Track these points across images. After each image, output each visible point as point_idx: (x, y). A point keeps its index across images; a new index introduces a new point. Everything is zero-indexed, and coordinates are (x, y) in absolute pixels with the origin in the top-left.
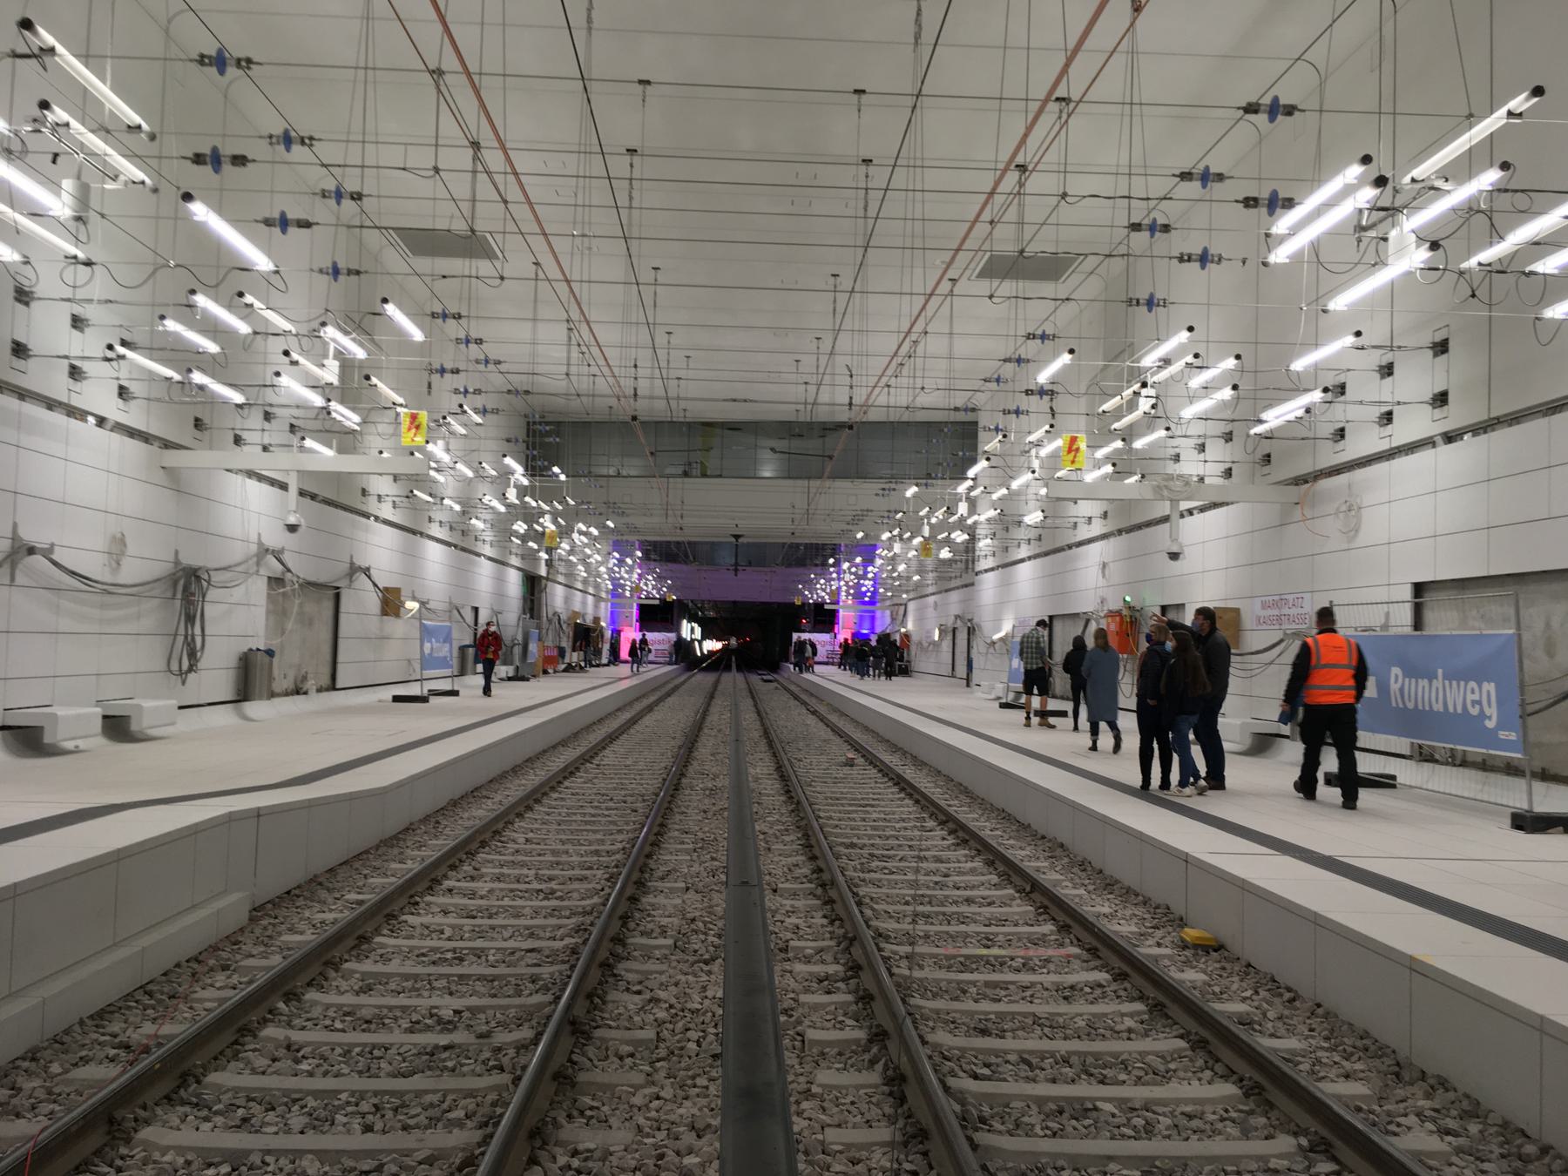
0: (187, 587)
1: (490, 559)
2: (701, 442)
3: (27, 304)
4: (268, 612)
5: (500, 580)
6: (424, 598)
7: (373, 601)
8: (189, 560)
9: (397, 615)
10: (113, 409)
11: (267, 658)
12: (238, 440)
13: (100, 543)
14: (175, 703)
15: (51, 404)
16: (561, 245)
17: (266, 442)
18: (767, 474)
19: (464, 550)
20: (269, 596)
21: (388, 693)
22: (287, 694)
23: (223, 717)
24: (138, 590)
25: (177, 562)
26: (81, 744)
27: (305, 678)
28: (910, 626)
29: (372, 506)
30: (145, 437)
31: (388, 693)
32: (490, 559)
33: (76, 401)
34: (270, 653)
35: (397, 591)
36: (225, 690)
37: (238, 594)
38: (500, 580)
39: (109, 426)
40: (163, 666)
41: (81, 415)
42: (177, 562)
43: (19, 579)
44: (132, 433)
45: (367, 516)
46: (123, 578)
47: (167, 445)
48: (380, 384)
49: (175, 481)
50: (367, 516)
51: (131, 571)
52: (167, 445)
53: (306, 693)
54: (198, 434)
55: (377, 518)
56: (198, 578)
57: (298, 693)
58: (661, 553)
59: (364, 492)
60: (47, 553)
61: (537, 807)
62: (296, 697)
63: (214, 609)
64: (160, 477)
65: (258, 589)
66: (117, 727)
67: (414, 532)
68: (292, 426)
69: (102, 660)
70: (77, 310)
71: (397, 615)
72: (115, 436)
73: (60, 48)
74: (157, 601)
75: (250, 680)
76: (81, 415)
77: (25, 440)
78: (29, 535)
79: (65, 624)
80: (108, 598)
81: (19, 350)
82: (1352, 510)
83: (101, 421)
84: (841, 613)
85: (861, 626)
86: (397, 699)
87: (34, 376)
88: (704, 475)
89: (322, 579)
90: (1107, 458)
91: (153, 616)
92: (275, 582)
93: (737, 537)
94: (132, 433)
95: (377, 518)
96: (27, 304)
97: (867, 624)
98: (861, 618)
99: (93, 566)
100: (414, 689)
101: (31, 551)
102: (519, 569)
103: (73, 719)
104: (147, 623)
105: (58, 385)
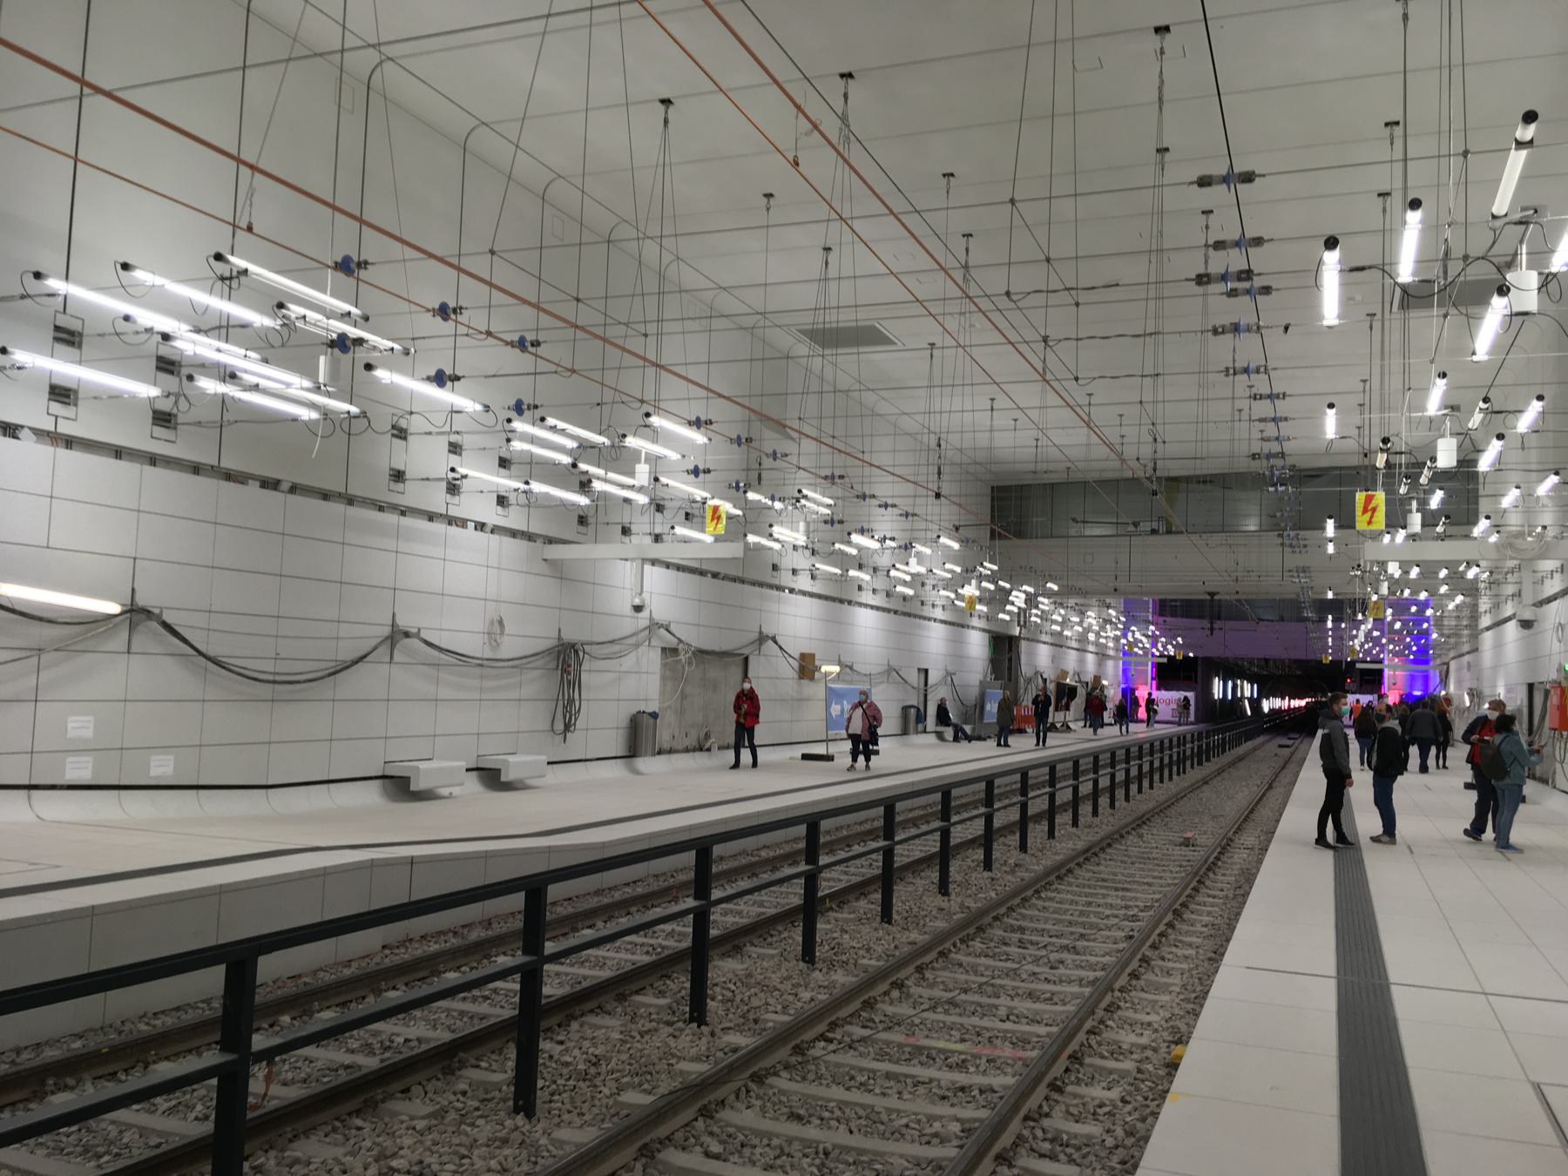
0: (566, 659)
1: (942, 622)
2: (1169, 497)
3: (405, 439)
4: (663, 678)
5: (957, 644)
6: (846, 659)
7: (788, 670)
8: (569, 636)
9: (812, 678)
10: (493, 515)
11: (651, 721)
12: (626, 531)
13: (480, 625)
14: (544, 758)
15: (431, 517)
16: (951, 323)
17: (657, 531)
18: (1252, 528)
19: (905, 614)
20: (664, 665)
21: (799, 751)
22: (687, 750)
23: (615, 770)
24: (520, 663)
25: (559, 638)
26: (456, 791)
27: (707, 736)
28: (1452, 688)
29: (786, 579)
30: (529, 537)
31: (799, 751)
32: (942, 622)
33: (453, 512)
34: (654, 715)
35: (813, 656)
36: (616, 745)
37: (628, 662)
38: (957, 644)
39: (488, 529)
40: (548, 727)
41: (462, 523)
42: (559, 638)
43: (397, 658)
44: (514, 534)
45: (780, 588)
46: (504, 653)
47: (550, 541)
48: (671, 483)
49: (558, 570)
50: (780, 588)
51: (510, 647)
52: (550, 541)
53: (709, 750)
54: (581, 529)
55: (792, 591)
56: (576, 652)
57: (701, 749)
58: (1171, 610)
59: (775, 567)
60: (417, 635)
61: (1078, 871)
62: (697, 754)
63: (593, 678)
64: (543, 568)
65: (651, 659)
66: (491, 778)
67: (841, 601)
68: (687, 514)
69: (507, 722)
70: (454, 438)
71: (812, 678)
72: (495, 539)
73: (252, 268)
74: (538, 672)
75: (638, 738)
76: (462, 523)
77: (403, 547)
78: (403, 622)
79: (445, 693)
80: (485, 671)
81: (398, 476)
82: (779, 600)
83: (480, 526)
84: (1387, 672)
85: (1412, 687)
86: (805, 757)
87: (411, 495)
88: (1169, 532)
89: (725, 647)
90: (849, 543)
91: (537, 684)
92: (669, 652)
93: (1212, 594)
94: (514, 534)
95: (792, 591)
96: (405, 439)
97: (1419, 683)
98: (1412, 678)
99: (472, 644)
100: (820, 749)
101: (407, 635)
102: (984, 630)
103: (439, 767)
104: (528, 691)
105: (437, 499)
